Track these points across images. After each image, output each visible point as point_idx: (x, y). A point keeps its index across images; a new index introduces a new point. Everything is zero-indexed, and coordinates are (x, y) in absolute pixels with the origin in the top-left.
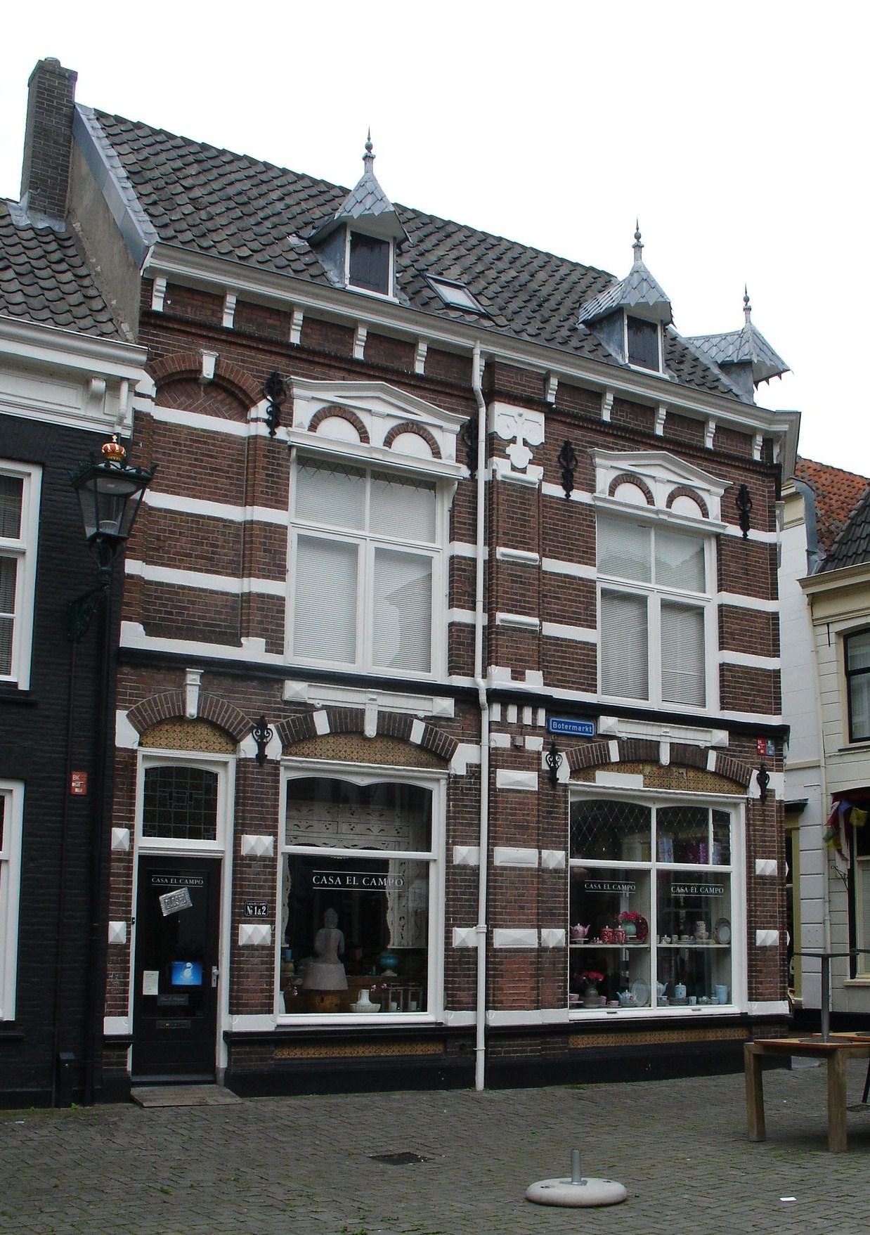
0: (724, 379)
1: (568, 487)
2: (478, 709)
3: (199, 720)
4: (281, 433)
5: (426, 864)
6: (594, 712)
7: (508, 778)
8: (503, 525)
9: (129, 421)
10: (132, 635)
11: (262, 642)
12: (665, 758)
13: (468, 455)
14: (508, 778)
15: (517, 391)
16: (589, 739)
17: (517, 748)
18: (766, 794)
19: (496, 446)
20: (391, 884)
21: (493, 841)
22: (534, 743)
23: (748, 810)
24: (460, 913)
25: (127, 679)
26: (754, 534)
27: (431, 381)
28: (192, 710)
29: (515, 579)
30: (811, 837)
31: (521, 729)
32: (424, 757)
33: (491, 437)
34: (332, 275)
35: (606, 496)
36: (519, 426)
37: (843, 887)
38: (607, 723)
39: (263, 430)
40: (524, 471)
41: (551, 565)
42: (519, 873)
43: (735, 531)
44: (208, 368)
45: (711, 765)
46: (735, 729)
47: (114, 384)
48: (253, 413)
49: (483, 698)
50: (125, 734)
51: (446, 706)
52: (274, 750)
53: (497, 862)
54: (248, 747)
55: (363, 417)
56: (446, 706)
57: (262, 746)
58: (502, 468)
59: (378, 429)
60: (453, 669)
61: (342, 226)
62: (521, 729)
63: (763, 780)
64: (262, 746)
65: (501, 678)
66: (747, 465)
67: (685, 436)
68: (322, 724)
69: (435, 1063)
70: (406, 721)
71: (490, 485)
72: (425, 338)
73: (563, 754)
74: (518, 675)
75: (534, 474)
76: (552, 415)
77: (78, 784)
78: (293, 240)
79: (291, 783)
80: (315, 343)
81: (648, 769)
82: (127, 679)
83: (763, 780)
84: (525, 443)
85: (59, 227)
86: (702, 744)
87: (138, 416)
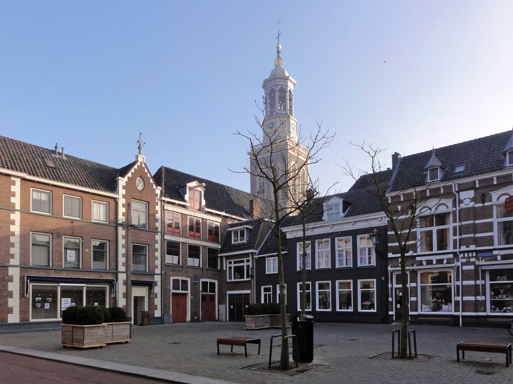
2: (458, 256)
7: (465, 268)
10: (390, 255)
11: (474, 246)
13: (454, 205)
14: (465, 268)
16: (491, 256)
19: (460, 202)
21: (462, 280)
22: (472, 260)
33: (459, 200)
38: (495, 252)
49: (458, 253)
51: (451, 256)
58: (463, 206)
62: (469, 257)
65: (464, 248)
75: (472, 204)
77: (383, 279)
84: (468, 198)
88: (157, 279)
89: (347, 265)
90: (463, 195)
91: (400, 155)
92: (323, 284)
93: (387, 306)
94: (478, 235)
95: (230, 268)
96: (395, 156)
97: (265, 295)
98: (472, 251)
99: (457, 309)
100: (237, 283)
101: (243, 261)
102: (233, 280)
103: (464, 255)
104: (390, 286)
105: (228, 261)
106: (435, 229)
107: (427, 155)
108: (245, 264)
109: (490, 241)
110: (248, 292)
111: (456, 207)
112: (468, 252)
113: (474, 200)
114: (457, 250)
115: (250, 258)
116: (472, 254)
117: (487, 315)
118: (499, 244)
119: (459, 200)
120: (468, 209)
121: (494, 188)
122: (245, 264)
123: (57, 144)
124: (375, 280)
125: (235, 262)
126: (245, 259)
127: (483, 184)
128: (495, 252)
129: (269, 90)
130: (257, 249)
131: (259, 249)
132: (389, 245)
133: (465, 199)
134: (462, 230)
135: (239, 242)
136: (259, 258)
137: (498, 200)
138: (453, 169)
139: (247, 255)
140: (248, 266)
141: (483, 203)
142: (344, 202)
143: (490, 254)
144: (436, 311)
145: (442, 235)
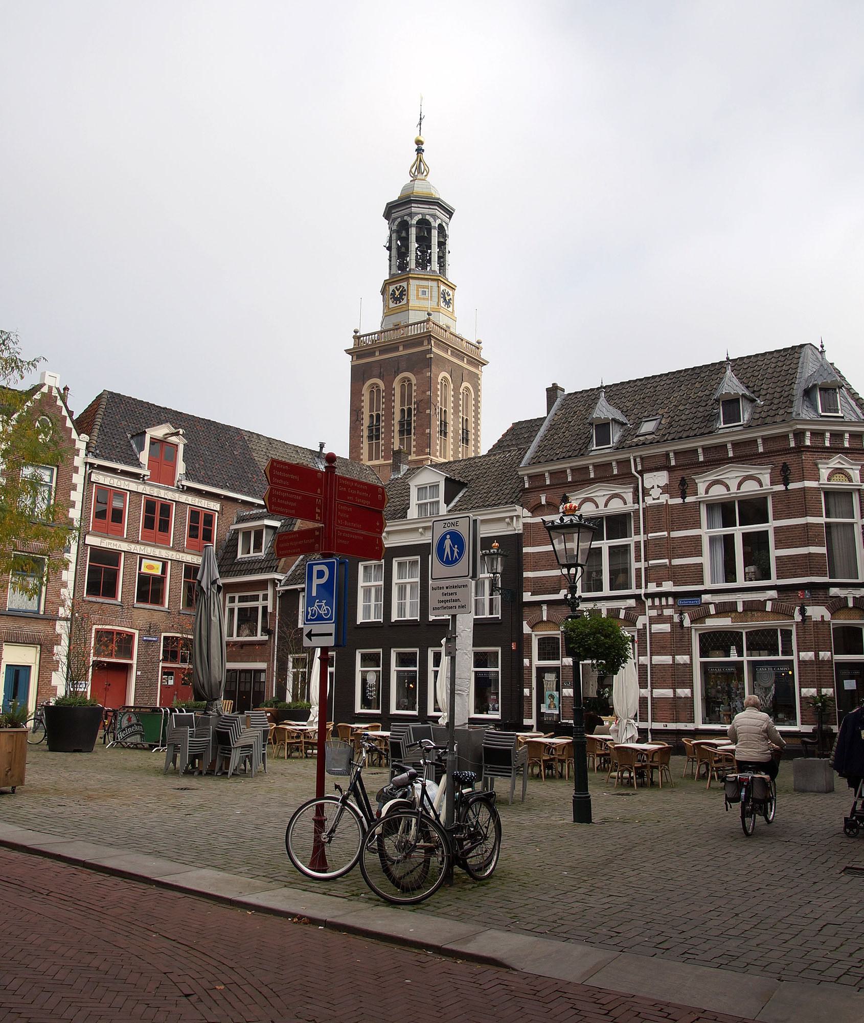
7: (656, 628)
9: (521, 527)
10: (527, 597)
11: (671, 583)
12: (740, 608)
13: (636, 500)
14: (656, 628)
16: (699, 606)
18: (805, 618)
22: (667, 612)
23: (797, 628)
25: (526, 611)
26: (791, 486)
27: (708, 462)
28: (545, 619)
29: (656, 545)
31: (661, 607)
32: (627, 624)
35: (826, 482)
38: (706, 598)
40: (658, 499)
41: (675, 534)
42: (663, 666)
43: (781, 487)
49: (643, 598)
50: (526, 629)
51: (632, 603)
55: (726, 481)
56: (632, 603)
58: (649, 501)
59: (601, 502)
62: (661, 607)
63: (803, 612)
65: (652, 588)
67: (747, 451)
70: (618, 610)
72: (828, 430)
73: (686, 615)
75: (664, 499)
80: (556, 481)
81: (733, 615)
82: (526, 611)
83: (803, 612)
84: (658, 486)
86: (762, 599)
87: (524, 524)
88: (62, 628)
89: (491, 613)
91: (563, 390)
92: (485, 653)
93: (521, 706)
94: (676, 562)
95: (232, 611)
96: (553, 392)
97: (295, 676)
98: (666, 595)
100: (243, 645)
101: (256, 598)
102: (235, 638)
103: (653, 602)
104: (526, 662)
105: (228, 596)
107: (716, 369)
108: (260, 604)
109: (696, 574)
110: (262, 665)
111: (638, 503)
112: (660, 595)
113: (666, 489)
114: (642, 591)
115: (270, 592)
116: (667, 600)
117: (697, 730)
118: (713, 582)
120: (660, 506)
121: (697, 470)
122: (260, 604)
123: (415, 232)
124: (499, 649)
125: (242, 599)
126: (261, 594)
127: (683, 460)
128: (706, 598)
129: (396, 223)
130: (283, 572)
131: (290, 573)
133: (653, 487)
134: (652, 549)
135: (252, 554)
136: (286, 591)
137: (606, 506)
138: (638, 425)
139: (263, 584)
140: (265, 608)
141: (684, 498)
142: (447, 479)
143: (695, 601)
144: (481, 713)
145: (756, 546)
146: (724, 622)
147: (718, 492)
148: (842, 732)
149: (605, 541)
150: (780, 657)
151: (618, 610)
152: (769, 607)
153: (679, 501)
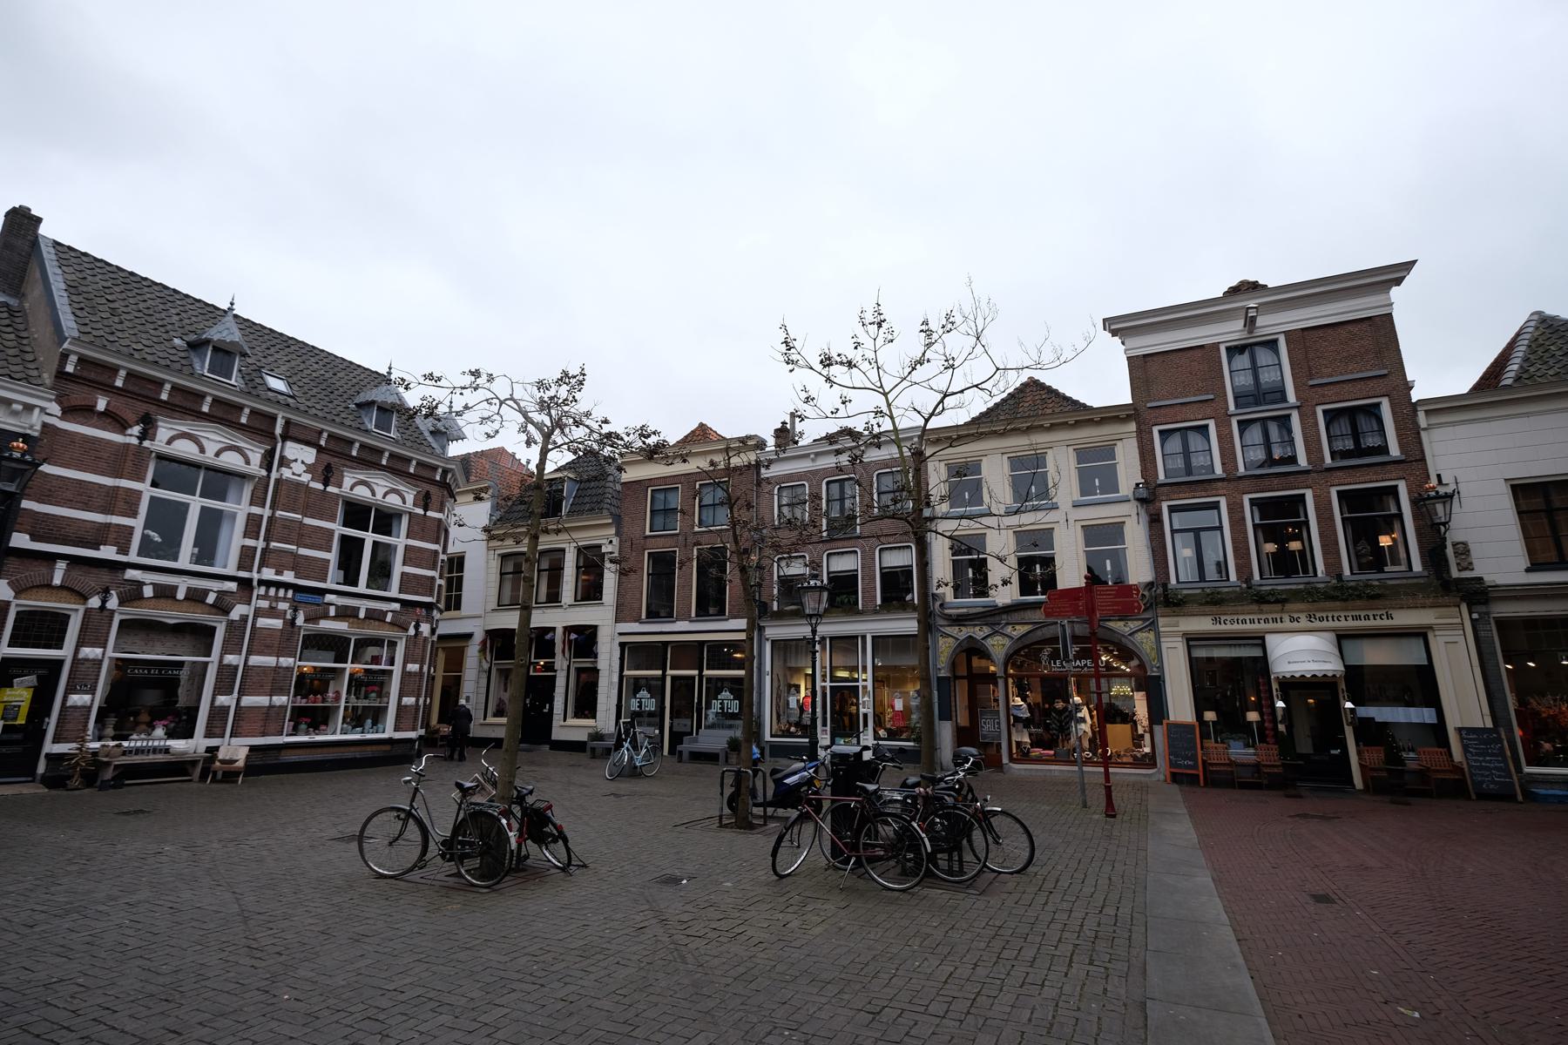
0: (430, 439)
1: (326, 484)
2: (251, 588)
3: (61, 587)
4: (146, 444)
5: (207, 663)
6: (323, 592)
7: (263, 622)
8: (282, 500)
9: (38, 427)
10: (20, 540)
12: (362, 615)
13: (267, 463)
14: (263, 622)
15: (302, 437)
17: (271, 607)
18: (417, 633)
19: (284, 462)
20: (184, 674)
22: (283, 606)
24: (223, 686)
29: (285, 527)
30: (472, 652)
33: (282, 458)
34: (197, 366)
36: (300, 456)
37: (485, 676)
38: (329, 598)
39: (135, 441)
42: (263, 669)
44: (101, 405)
45: (388, 619)
46: (404, 603)
47: (29, 408)
48: (129, 431)
49: (255, 583)
52: (113, 603)
53: (250, 663)
54: (95, 602)
56: (233, 586)
57: (104, 602)
59: (380, 492)
60: (240, 568)
61: (208, 342)
62: (277, 599)
63: (417, 627)
64: (104, 602)
65: (269, 574)
66: (433, 482)
67: (399, 466)
68: (148, 592)
69: (207, 767)
71: (278, 481)
74: (278, 573)
75: (306, 478)
76: (320, 449)
78: (177, 341)
79: (122, 622)
80: (178, 400)
83: (417, 627)
85: (13, 302)
87: (45, 425)
90: (293, 450)
94: (303, 551)
98: (287, 586)
99: (217, 731)
106: (369, 537)
112: (279, 585)
113: (310, 469)
119: (282, 458)
120: (299, 485)
132: (25, 504)
137: (169, 443)
143: (317, 599)
146: (341, 626)
147: (362, 493)
148: (1273, 704)
149: (197, 498)
150: (383, 667)
151: (206, 592)
152: (389, 618)
153: (320, 486)
